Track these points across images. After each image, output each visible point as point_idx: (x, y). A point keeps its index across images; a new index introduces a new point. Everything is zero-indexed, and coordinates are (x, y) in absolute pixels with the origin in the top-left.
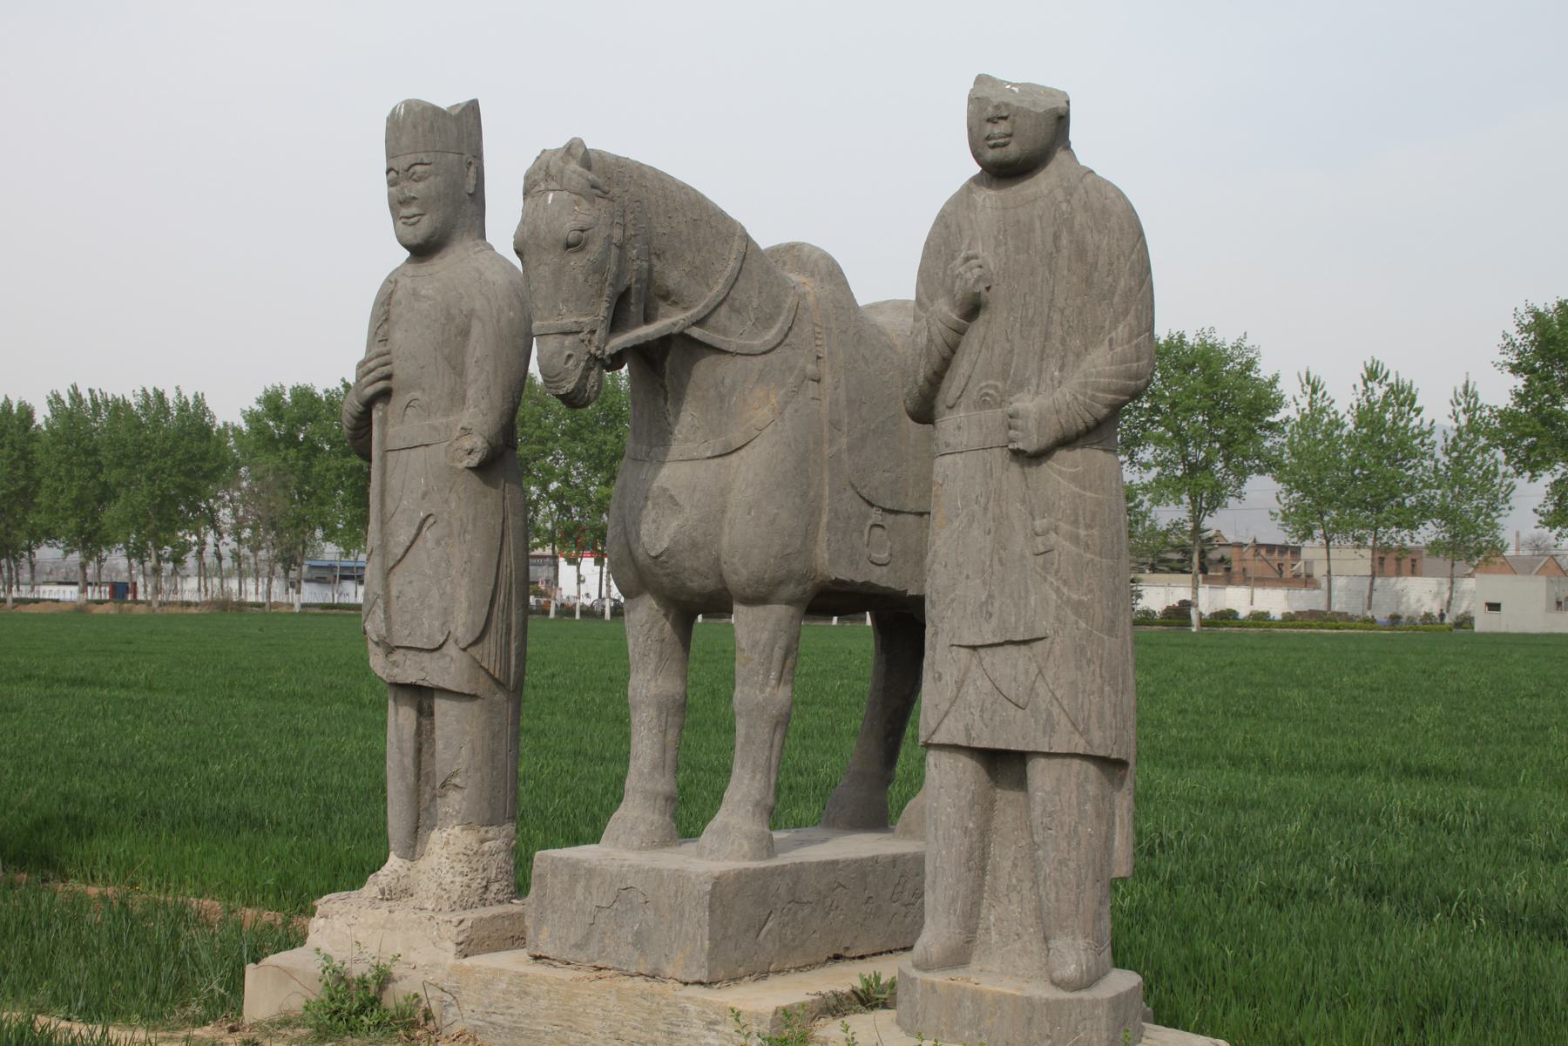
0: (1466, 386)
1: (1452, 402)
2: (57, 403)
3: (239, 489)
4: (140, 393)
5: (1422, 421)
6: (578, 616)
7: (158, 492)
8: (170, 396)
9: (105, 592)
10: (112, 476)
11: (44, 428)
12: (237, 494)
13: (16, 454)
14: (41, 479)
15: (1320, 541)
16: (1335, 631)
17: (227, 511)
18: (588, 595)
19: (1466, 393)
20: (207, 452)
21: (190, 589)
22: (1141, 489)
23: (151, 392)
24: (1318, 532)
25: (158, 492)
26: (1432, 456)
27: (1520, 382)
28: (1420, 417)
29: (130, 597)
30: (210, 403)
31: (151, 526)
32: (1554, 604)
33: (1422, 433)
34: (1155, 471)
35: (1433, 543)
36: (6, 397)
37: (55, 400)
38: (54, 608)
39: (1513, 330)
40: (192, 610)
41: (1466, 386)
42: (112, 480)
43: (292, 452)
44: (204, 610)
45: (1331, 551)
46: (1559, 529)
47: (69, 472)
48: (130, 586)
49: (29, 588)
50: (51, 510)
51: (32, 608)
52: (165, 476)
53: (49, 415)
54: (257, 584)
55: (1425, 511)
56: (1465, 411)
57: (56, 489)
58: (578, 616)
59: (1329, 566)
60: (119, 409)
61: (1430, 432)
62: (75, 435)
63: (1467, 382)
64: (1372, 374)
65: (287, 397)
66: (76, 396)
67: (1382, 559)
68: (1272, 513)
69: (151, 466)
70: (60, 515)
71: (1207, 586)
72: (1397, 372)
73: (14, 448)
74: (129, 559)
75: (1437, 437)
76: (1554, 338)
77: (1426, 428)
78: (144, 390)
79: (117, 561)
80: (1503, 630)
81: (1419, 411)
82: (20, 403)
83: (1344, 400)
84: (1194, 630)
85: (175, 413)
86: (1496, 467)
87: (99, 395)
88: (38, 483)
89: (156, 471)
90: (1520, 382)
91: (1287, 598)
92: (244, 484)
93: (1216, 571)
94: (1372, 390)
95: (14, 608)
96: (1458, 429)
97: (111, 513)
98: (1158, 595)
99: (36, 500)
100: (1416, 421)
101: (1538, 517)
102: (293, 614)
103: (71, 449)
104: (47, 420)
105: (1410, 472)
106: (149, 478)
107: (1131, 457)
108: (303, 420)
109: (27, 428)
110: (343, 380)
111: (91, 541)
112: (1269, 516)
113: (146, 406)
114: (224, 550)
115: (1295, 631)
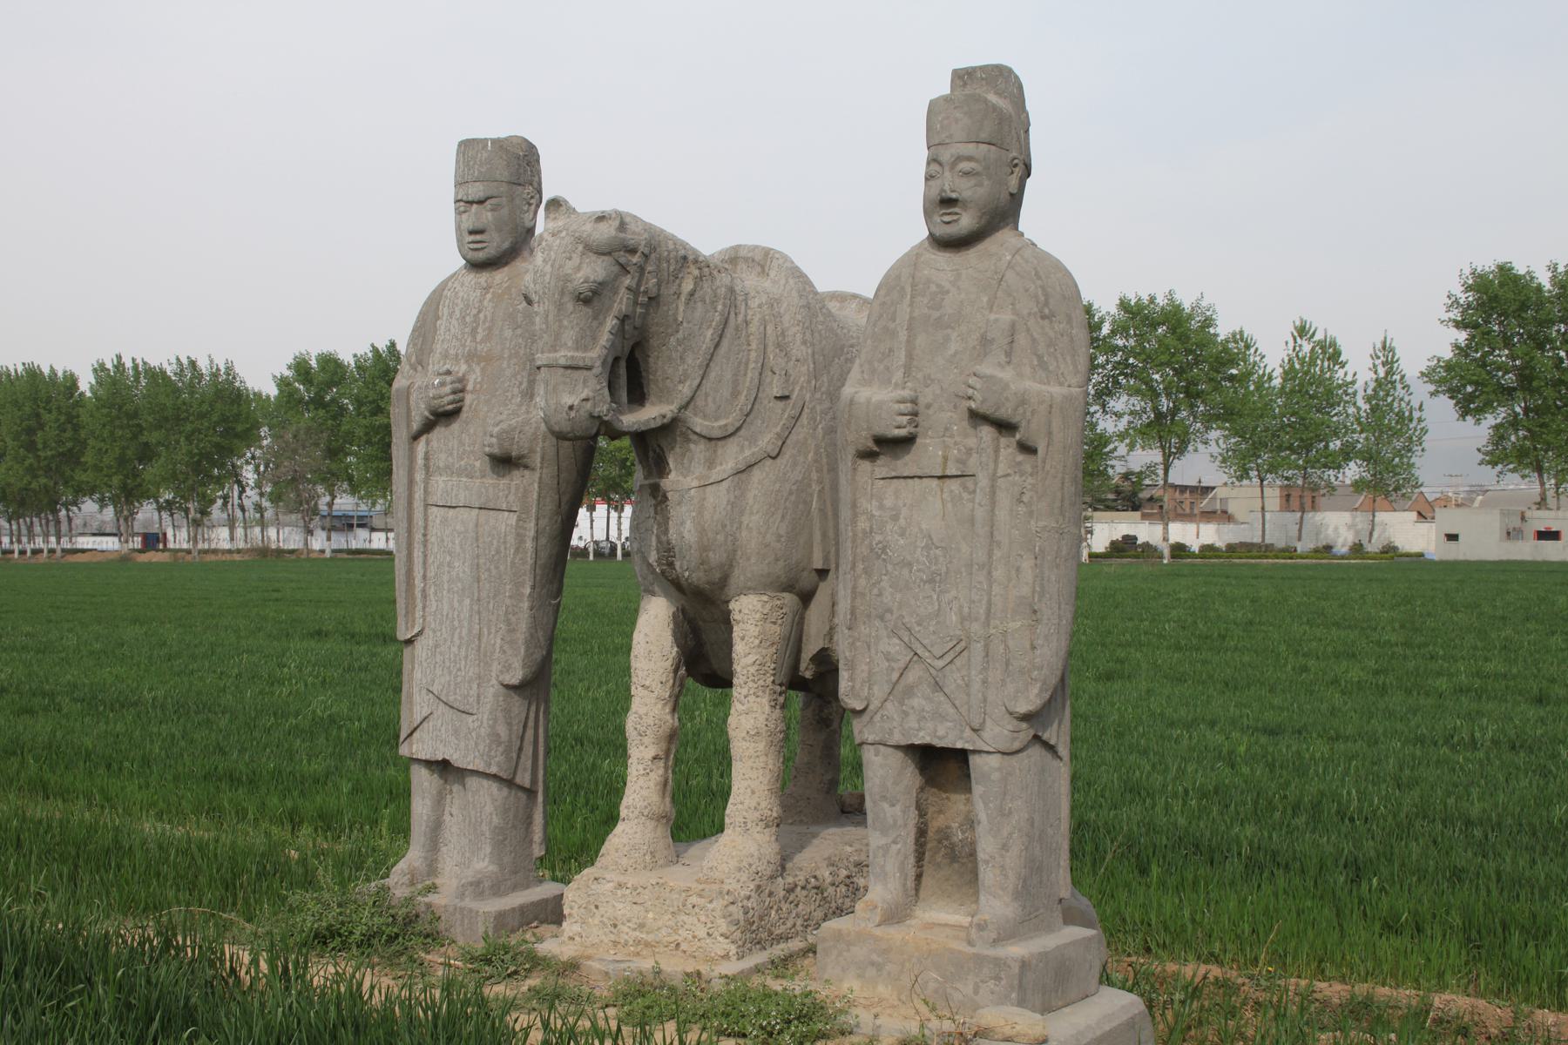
0: (1385, 342)
1: (1371, 356)
2: (102, 371)
3: (261, 447)
4: (175, 361)
5: (1346, 374)
6: (591, 558)
7: (196, 451)
8: (203, 365)
9: (137, 542)
10: (153, 437)
11: (89, 394)
12: (258, 453)
13: (63, 418)
14: (85, 440)
15: (1256, 481)
16: (1289, 561)
17: (250, 467)
18: (581, 538)
19: (1384, 348)
20: (239, 415)
21: (221, 538)
22: (1117, 436)
23: (185, 361)
24: (1253, 473)
25: (196, 451)
26: (1355, 404)
27: (1462, 336)
28: (1345, 369)
29: (161, 546)
30: (239, 369)
31: (190, 482)
32: (1505, 535)
33: (1347, 384)
34: (1126, 419)
35: (1356, 481)
36: (51, 367)
37: (100, 369)
38: (99, 557)
39: (1458, 291)
40: (237, 557)
41: (1385, 342)
42: (154, 441)
43: (321, 413)
44: (247, 557)
45: (1265, 489)
46: (1500, 466)
47: (112, 433)
48: (160, 536)
49: (67, 539)
50: (97, 469)
51: (212, 557)
52: (202, 436)
53: (93, 382)
54: (278, 533)
55: (1347, 454)
56: (1384, 364)
57: (100, 449)
58: (591, 558)
59: (1263, 503)
60: (156, 376)
61: (1353, 382)
62: (118, 400)
63: (1385, 338)
64: (1302, 331)
65: (313, 363)
66: (119, 366)
67: (1288, 496)
68: (1212, 456)
69: (189, 427)
70: (104, 472)
71: (1147, 522)
72: (1325, 330)
73: (60, 413)
74: (160, 512)
75: (1359, 385)
76: (1496, 296)
77: (1349, 379)
78: (178, 359)
79: (146, 514)
80: (1461, 558)
81: (1343, 365)
82: (65, 372)
83: (20, 368)
84: (1165, 561)
85: (208, 378)
86: (1411, 413)
87: (141, 364)
88: (84, 444)
89: (193, 433)
90: (1462, 336)
91: (1218, 531)
92: (265, 442)
93: (1152, 509)
94: (1300, 346)
95: (62, 557)
96: (1377, 380)
97: (150, 472)
98: (1105, 531)
99: (82, 460)
100: (1341, 373)
101: (1481, 456)
102: (326, 559)
103: (114, 412)
104: (92, 387)
105: (1335, 419)
106: (187, 438)
107: (1104, 406)
108: (330, 384)
109: (72, 395)
110: (373, 346)
111: (129, 495)
112: (1209, 458)
113: (180, 373)
114: (247, 503)
115: (1253, 561)
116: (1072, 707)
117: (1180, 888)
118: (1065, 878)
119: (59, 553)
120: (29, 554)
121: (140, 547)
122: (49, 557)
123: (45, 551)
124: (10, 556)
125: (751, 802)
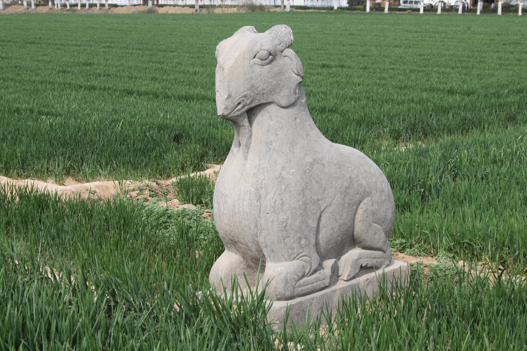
6: (520, 13)
58: (520, 13)
95: (109, 9)
116: (356, 5)
117: (506, 313)
118: (406, 6)
119: (107, 7)
120: (87, 7)
121: (347, 5)
122: (100, 9)
123: (98, 5)
124: (75, 8)
125: (40, 187)
